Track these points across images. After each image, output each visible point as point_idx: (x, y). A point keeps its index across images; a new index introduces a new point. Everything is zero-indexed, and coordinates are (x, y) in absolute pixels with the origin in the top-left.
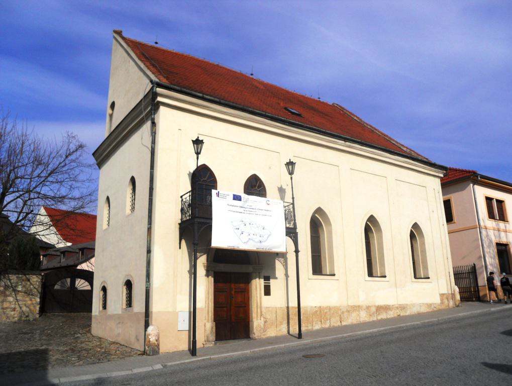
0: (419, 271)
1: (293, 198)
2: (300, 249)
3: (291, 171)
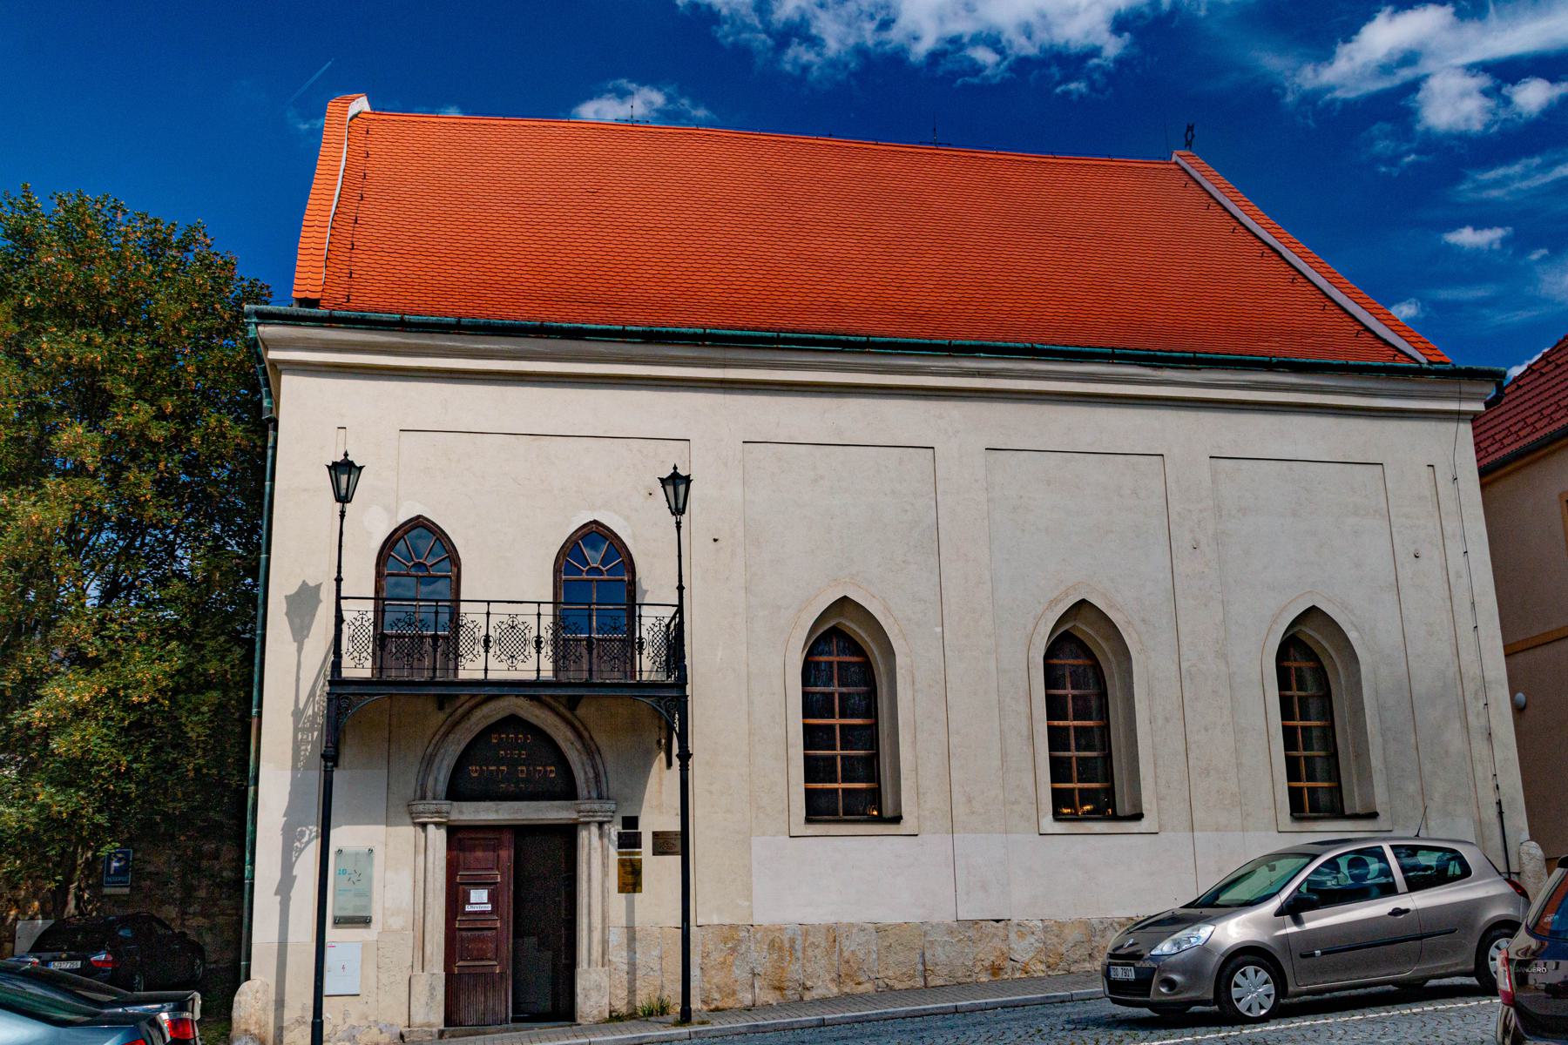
0: (1089, 775)
1: (681, 588)
3: (343, 492)
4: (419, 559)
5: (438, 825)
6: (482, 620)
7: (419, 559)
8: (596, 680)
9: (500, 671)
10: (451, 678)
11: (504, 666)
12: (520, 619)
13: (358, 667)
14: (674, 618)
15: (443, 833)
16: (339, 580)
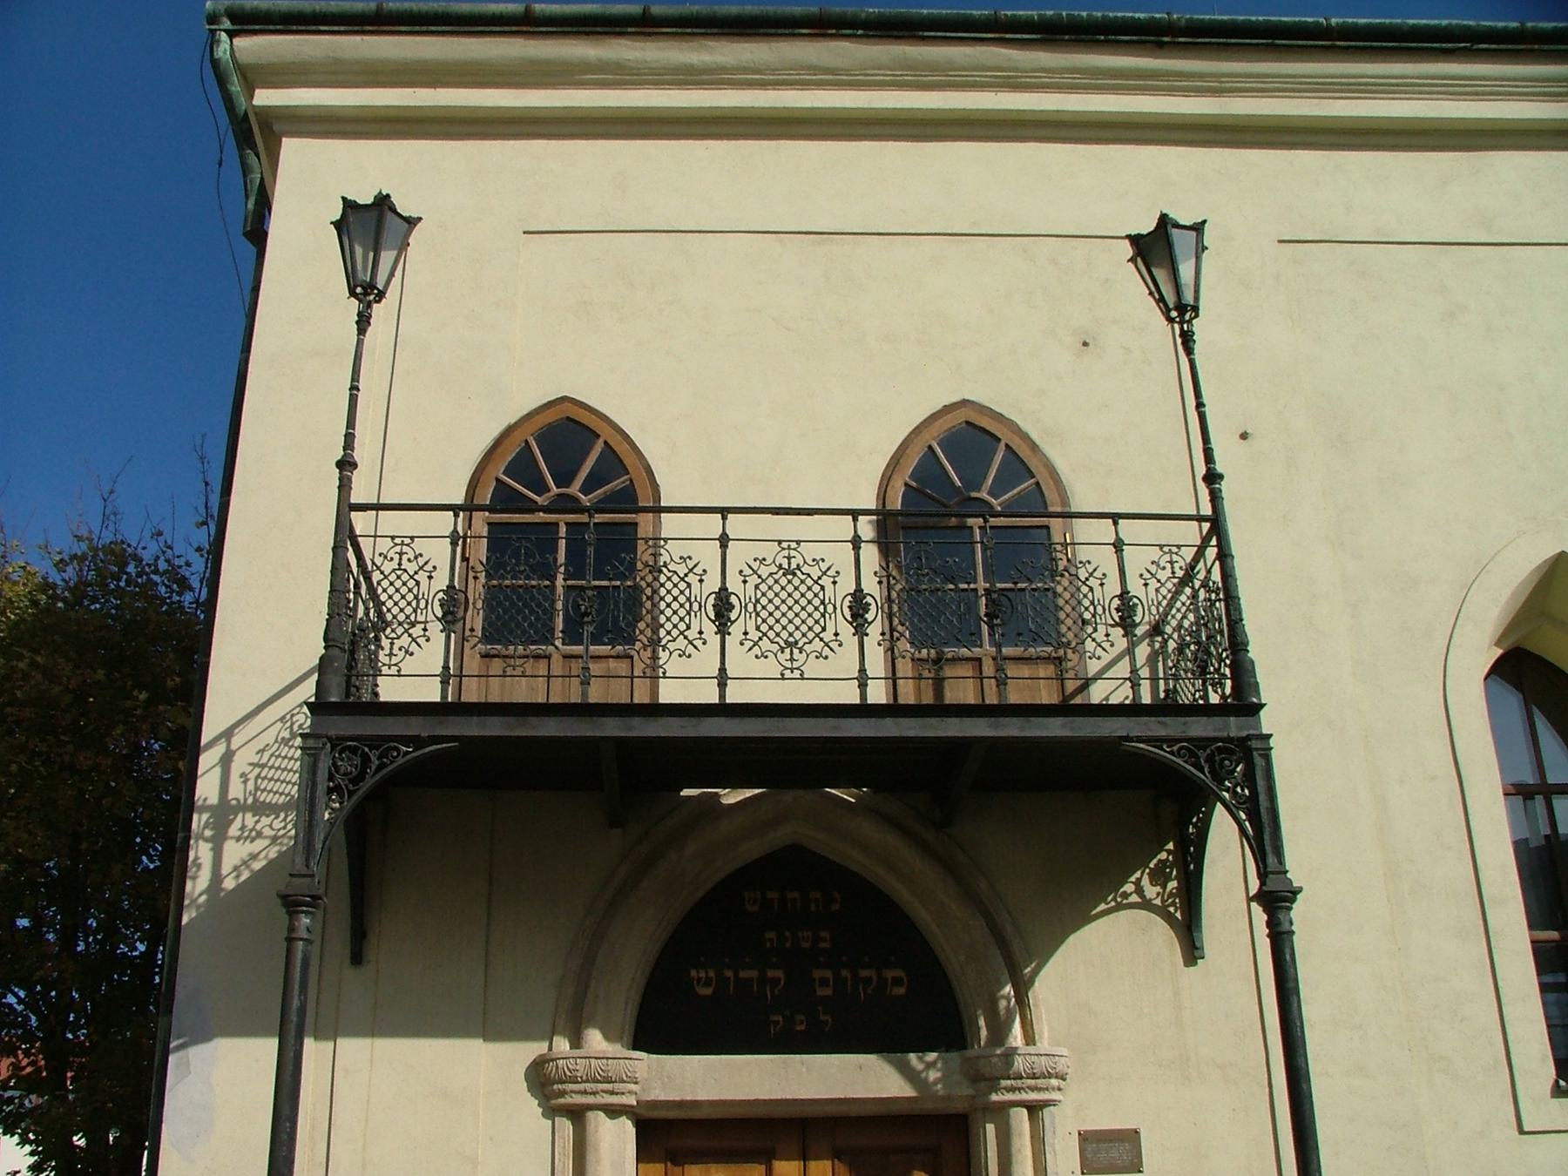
2: (1296, 873)
4: (565, 516)
5: (613, 1112)
6: (708, 555)
7: (565, 516)
8: (1013, 698)
9: (759, 681)
10: (641, 697)
11: (771, 667)
12: (810, 551)
13: (413, 673)
14: (1205, 542)
15: (627, 1128)
16: (346, 465)
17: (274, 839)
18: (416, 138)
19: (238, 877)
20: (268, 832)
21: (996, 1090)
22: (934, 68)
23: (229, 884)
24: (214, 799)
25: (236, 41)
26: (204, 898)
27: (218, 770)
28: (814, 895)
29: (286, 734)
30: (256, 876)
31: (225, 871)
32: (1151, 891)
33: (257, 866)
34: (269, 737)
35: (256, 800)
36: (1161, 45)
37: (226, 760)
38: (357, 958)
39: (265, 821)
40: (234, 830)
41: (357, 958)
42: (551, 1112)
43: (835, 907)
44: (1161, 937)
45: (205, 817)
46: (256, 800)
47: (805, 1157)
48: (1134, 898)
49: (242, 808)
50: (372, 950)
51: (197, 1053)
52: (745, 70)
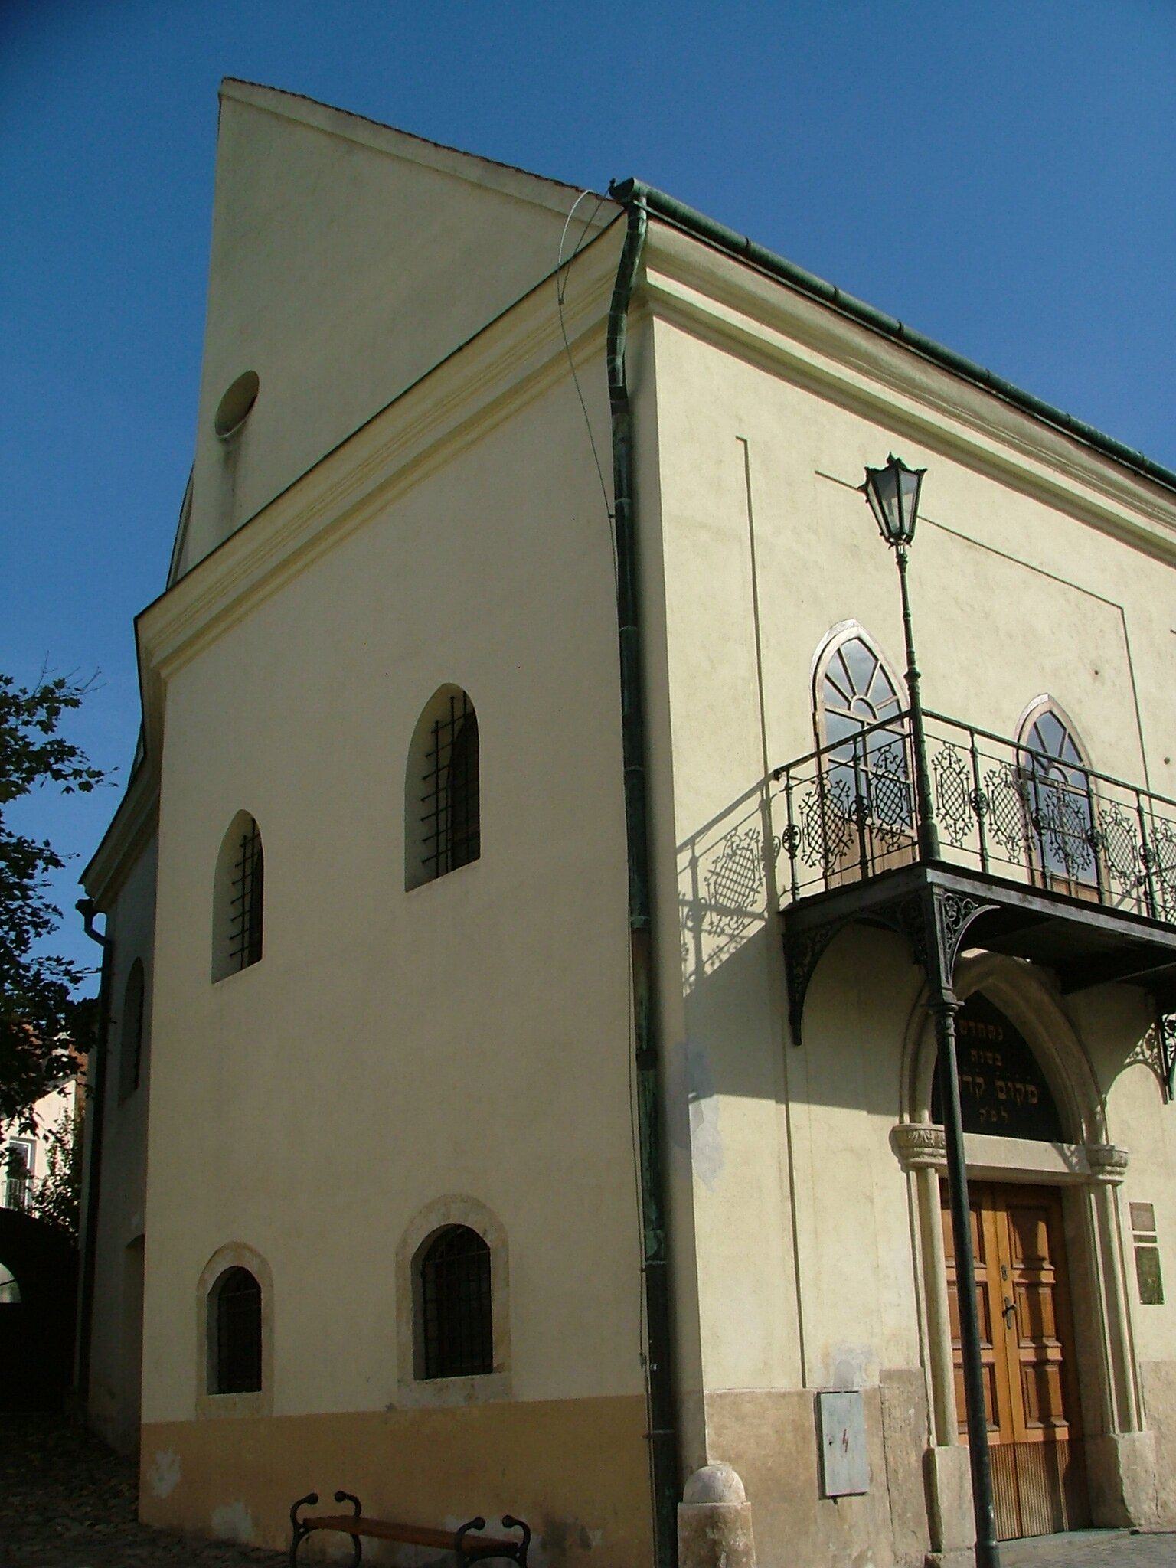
17: (732, 937)
18: (722, 350)
19: (712, 964)
20: (728, 930)
21: (1103, 1172)
22: (1033, 441)
23: (708, 969)
24: (689, 897)
25: (651, 223)
26: (692, 978)
27: (689, 871)
28: (991, 1028)
29: (729, 851)
30: (725, 965)
31: (705, 957)
32: (1148, 1053)
33: (724, 957)
34: (718, 851)
35: (717, 902)
36: (1136, 474)
37: (694, 863)
38: (797, 1040)
39: (726, 920)
40: (706, 926)
41: (797, 1040)
42: (906, 1167)
43: (7, 986)
44: (1153, 1082)
45: (686, 910)
46: (717, 902)
47: (994, 1209)
48: (1141, 1057)
49: (708, 907)
50: (806, 1032)
51: (705, 1103)
52: (940, 397)
